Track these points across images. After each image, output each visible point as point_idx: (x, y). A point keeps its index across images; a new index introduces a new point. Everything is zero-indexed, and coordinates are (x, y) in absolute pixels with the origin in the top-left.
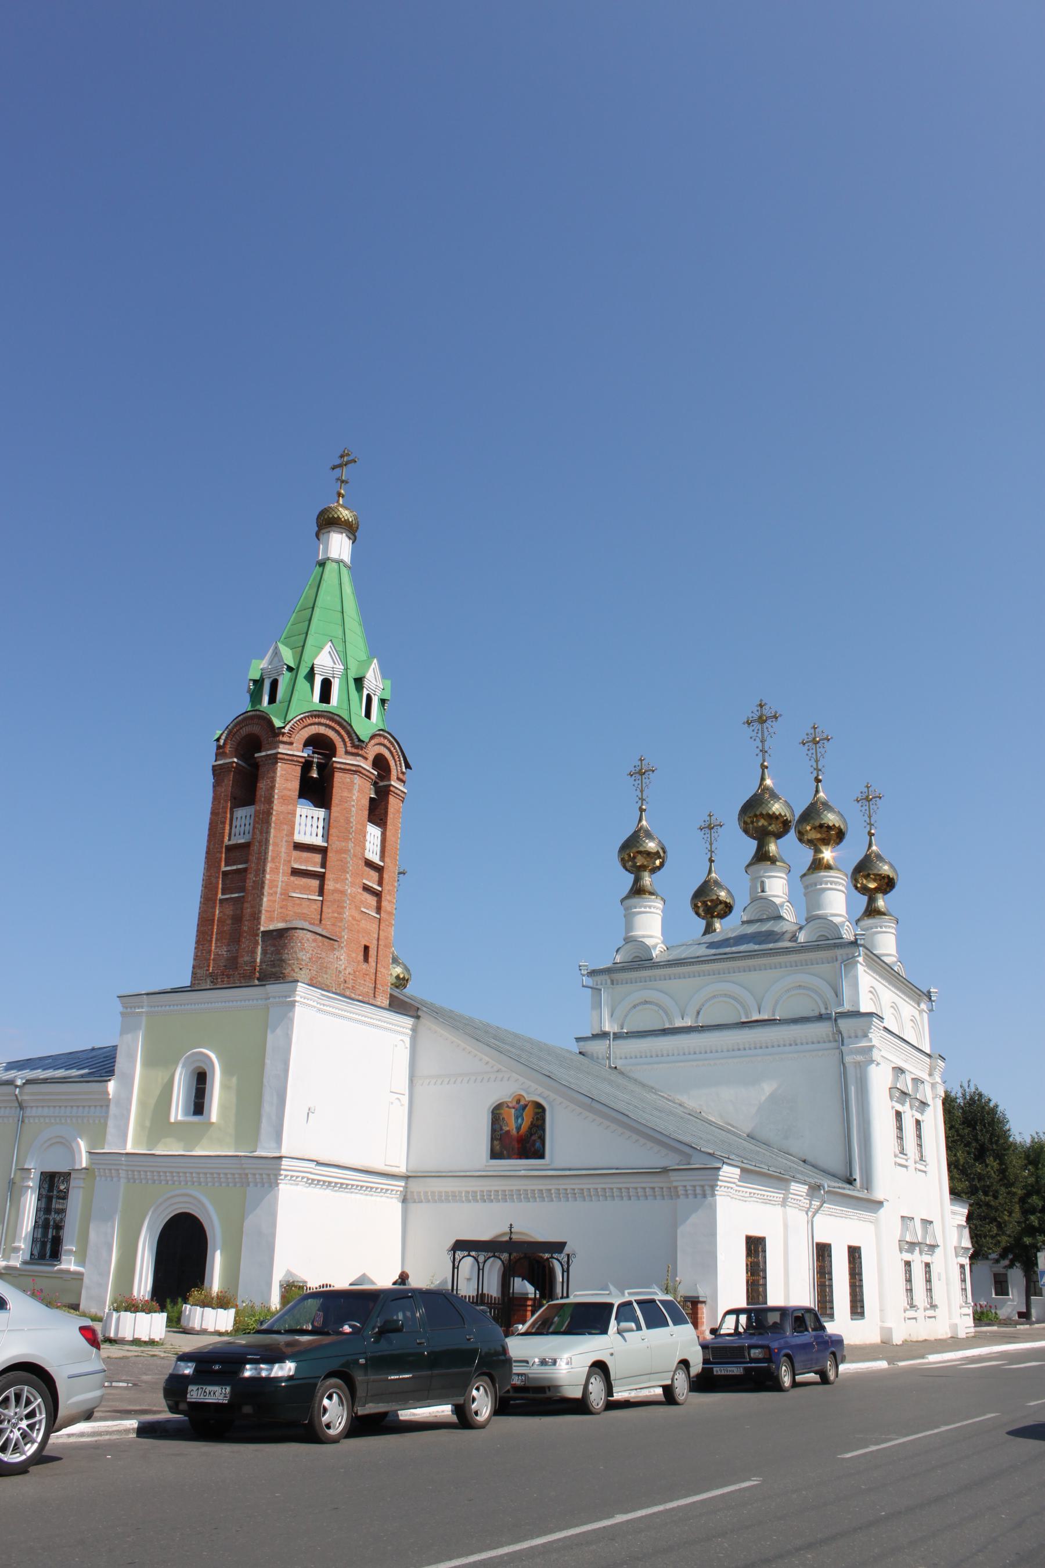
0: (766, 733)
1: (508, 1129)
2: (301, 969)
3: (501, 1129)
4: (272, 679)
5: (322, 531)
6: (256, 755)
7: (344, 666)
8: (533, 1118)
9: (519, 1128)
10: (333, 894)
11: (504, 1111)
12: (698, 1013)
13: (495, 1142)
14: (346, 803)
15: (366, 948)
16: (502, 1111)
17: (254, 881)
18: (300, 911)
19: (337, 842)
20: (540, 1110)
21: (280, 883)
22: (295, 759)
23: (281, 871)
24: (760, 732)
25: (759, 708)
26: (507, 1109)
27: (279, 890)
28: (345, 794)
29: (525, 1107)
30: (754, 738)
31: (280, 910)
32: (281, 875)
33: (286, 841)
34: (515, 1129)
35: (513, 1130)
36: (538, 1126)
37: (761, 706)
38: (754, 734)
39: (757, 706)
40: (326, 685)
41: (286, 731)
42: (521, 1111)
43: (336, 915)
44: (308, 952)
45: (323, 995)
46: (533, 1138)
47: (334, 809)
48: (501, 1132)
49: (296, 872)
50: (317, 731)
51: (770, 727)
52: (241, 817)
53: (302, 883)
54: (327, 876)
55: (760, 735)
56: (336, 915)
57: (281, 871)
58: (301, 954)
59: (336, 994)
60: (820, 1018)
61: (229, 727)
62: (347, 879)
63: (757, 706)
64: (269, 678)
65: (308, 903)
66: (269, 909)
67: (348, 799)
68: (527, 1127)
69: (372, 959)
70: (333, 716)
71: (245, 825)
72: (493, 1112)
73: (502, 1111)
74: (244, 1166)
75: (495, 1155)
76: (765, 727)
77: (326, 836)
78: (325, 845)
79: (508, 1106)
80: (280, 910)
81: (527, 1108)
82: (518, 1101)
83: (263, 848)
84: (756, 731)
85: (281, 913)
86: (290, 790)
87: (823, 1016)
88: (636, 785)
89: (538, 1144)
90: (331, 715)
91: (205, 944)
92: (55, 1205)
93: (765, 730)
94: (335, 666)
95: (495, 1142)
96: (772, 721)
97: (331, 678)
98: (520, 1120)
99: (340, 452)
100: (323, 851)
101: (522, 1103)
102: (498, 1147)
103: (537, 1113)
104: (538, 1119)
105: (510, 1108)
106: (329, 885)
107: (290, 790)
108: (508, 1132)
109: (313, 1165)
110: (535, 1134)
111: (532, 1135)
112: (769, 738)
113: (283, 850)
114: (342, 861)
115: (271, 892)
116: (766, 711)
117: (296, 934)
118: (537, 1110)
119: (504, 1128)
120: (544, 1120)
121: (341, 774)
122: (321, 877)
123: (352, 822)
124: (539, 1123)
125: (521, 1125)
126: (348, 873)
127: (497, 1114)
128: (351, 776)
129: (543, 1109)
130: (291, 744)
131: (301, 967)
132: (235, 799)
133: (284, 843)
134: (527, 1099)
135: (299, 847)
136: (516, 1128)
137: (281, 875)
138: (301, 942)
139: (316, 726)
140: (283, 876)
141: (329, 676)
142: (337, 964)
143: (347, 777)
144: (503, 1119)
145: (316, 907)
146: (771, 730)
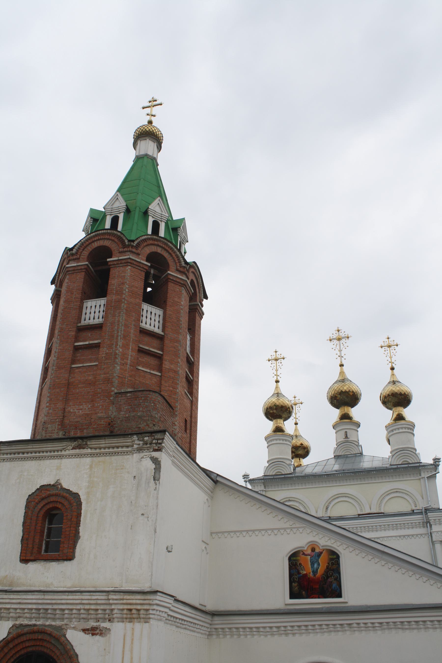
0: (342, 346)
1: (305, 572)
2: (154, 425)
3: (299, 573)
4: (113, 216)
5: (140, 139)
6: (108, 260)
7: (168, 214)
8: (328, 563)
9: (315, 572)
10: (169, 372)
11: (301, 558)
12: (327, 508)
13: (293, 584)
14: (177, 306)
15: (186, 421)
16: (299, 558)
17: (106, 354)
18: (143, 381)
19: (171, 334)
20: (335, 557)
21: (130, 357)
22: (141, 266)
23: (131, 347)
24: (338, 345)
25: (337, 332)
26: (303, 556)
27: (129, 361)
28: (176, 299)
29: (320, 554)
30: (334, 349)
31: (129, 378)
32: (130, 350)
33: (134, 325)
34: (311, 573)
35: (310, 573)
36: (333, 570)
37: (338, 331)
38: (334, 346)
39: (336, 331)
40: (156, 225)
41: (135, 245)
42: (317, 558)
43: (171, 389)
44: (159, 412)
45: (176, 447)
46: (329, 580)
47: (168, 308)
48: (299, 575)
49: (141, 351)
50: (156, 251)
51: (344, 343)
52: (91, 307)
53: (144, 360)
54: (165, 357)
55: (338, 347)
56: (171, 389)
57: (131, 347)
58: (154, 412)
59: (182, 449)
60: (413, 513)
61: (82, 241)
62: (178, 362)
63: (336, 331)
64: (111, 215)
65: (150, 376)
66: (120, 376)
67: (178, 303)
68: (323, 572)
69: (188, 431)
70: (167, 242)
71: (95, 312)
72: (290, 559)
73: (299, 558)
74: (111, 602)
75: (292, 596)
76: (341, 343)
77: (164, 328)
78: (162, 334)
79: (304, 554)
80: (129, 378)
81: (322, 555)
82: (313, 550)
83: (116, 328)
84: (335, 345)
85: (131, 380)
86: (137, 288)
87: (415, 511)
88: (273, 367)
89: (334, 585)
90: (166, 241)
91: (57, 403)
92: (128, 620)
93: (342, 345)
94: (162, 213)
95: (293, 584)
96: (346, 340)
97: (159, 221)
98: (316, 566)
99: (150, 99)
100: (160, 338)
101: (317, 550)
102: (297, 588)
103: (332, 559)
104: (333, 564)
105: (306, 555)
106: (166, 365)
107: (137, 288)
108: (306, 575)
109: (171, 601)
110: (331, 576)
111: (328, 577)
112: (344, 349)
113: (132, 331)
114: (175, 348)
115: (123, 362)
116: (342, 334)
117: (150, 396)
118: (332, 557)
119: (301, 572)
120: (338, 564)
121: (173, 284)
122: (159, 358)
123: (181, 321)
124: (335, 567)
125: (317, 570)
126: (179, 357)
127: (294, 560)
128: (180, 288)
129: (338, 557)
130: (138, 254)
131: (154, 423)
132: (85, 293)
133: (133, 326)
134: (321, 548)
135: (145, 332)
136: (313, 572)
137: (130, 350)
138: (154, 403)
139: (155, 247)
140: (132, 351)
141: (158, 219)
142: (173, 428)
143: (177, 288)
144: (300, 564)
145: (156, 380)
146: (345, 345)
